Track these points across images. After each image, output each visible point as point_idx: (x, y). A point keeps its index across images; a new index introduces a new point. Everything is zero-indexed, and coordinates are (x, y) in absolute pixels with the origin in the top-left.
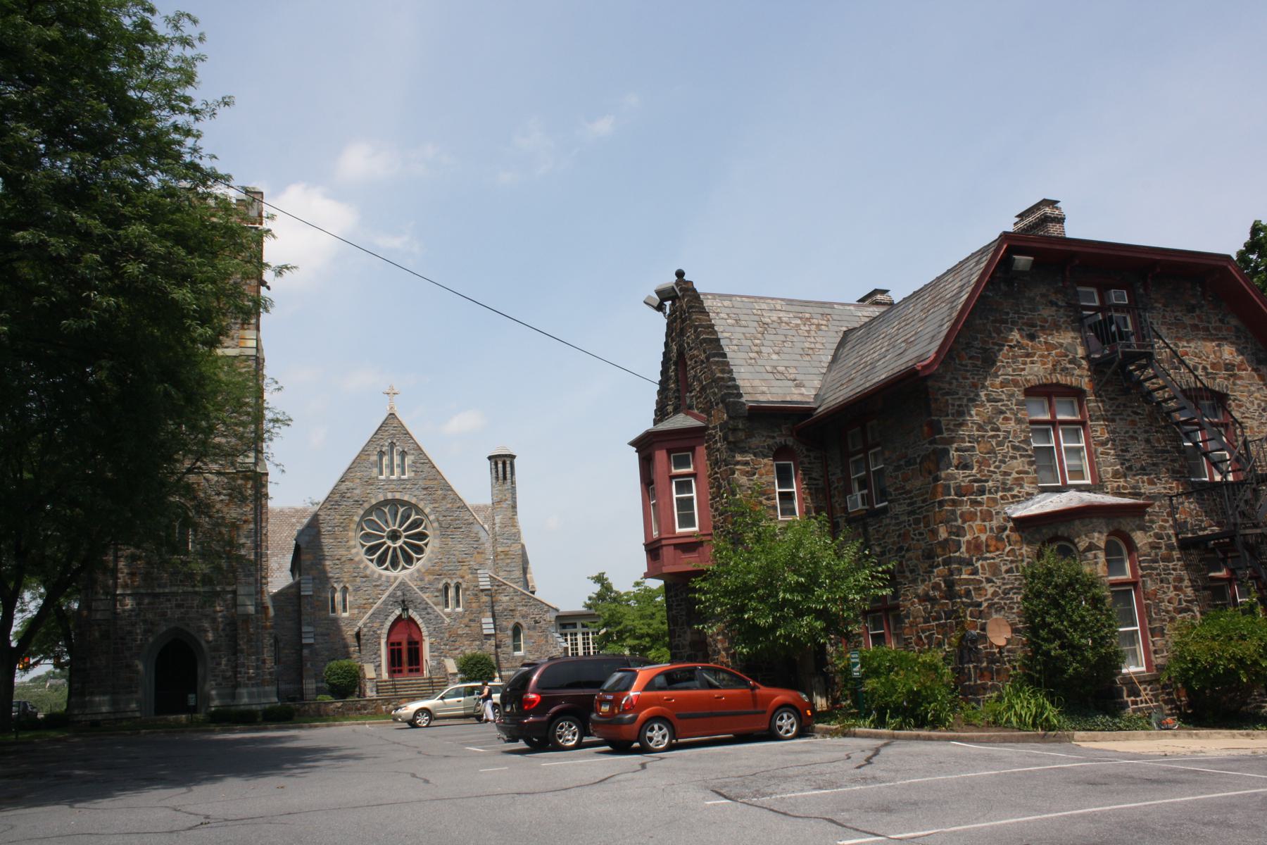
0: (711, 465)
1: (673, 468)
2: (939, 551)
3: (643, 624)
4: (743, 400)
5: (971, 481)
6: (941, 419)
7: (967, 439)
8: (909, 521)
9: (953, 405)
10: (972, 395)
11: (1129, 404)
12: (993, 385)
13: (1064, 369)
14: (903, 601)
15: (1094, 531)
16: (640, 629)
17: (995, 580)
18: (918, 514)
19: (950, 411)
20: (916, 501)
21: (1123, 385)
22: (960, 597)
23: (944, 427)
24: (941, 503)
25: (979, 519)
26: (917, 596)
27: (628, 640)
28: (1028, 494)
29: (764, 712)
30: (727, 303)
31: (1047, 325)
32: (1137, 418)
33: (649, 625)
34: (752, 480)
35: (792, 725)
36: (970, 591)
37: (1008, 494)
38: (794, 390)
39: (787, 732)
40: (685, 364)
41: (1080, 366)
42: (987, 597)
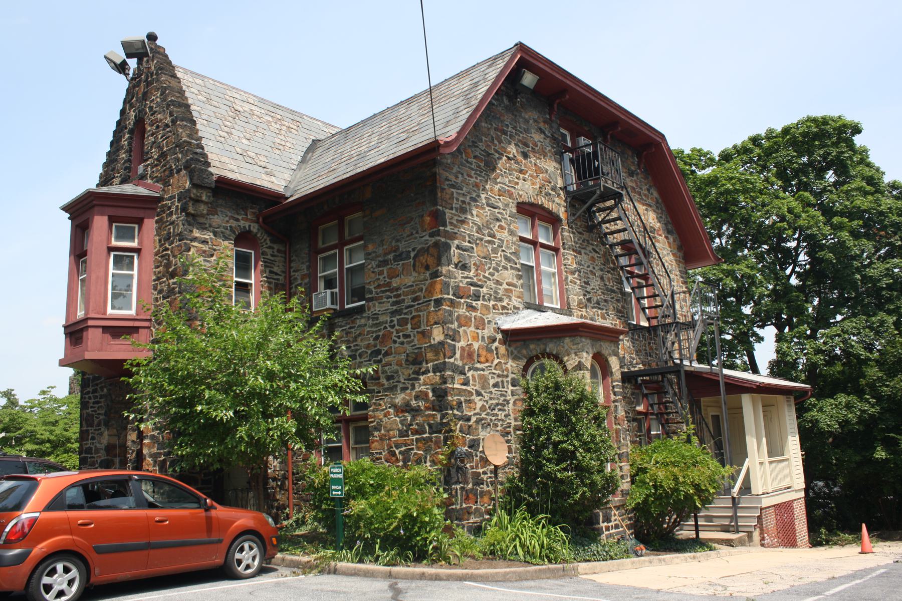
0: (160, 241)
1: (113, 239)
2: (430, 355)
3: (45, 430)
4: (210, 169)
5: (467, 283)
6: (447, 211)
7: (467, 239)
8: (392, 321)
9: (458, 200)
10: (474, 195)
11: (591, 242)
12: (492, 188)
13: (547, 194)
14: (373, 411)
15: (583, 351)
16: (42, 434)
17: (484, 394)
18: (405, 314)
19: (454, 206)
20: (404, 300)
21: (587, 223)
22: (452, 409)
23: (448, 221)
24: (438, 302)
25: (473, 325)
26: (394, 406)
27: (27, 444)
28: (515, 308)
29: (220, 541)
30: (198, 81)
31: (536, 148)
32: (596, 255)
33: (51, 432)
34: (208, 261)
35: (254, 558)
36: (461, 403)
37: (499, 304)
38: (267, 178)
39: (248, 567)
40: (143, 131)
41: (559, 195)
42: (476, 412)
